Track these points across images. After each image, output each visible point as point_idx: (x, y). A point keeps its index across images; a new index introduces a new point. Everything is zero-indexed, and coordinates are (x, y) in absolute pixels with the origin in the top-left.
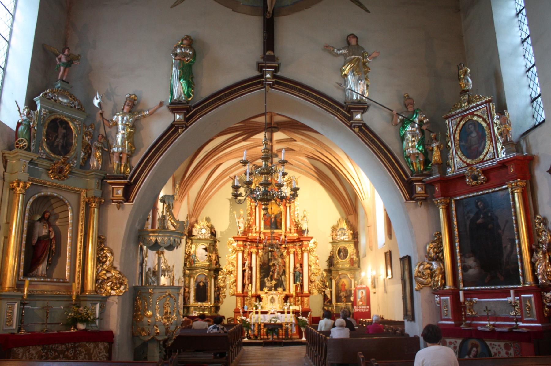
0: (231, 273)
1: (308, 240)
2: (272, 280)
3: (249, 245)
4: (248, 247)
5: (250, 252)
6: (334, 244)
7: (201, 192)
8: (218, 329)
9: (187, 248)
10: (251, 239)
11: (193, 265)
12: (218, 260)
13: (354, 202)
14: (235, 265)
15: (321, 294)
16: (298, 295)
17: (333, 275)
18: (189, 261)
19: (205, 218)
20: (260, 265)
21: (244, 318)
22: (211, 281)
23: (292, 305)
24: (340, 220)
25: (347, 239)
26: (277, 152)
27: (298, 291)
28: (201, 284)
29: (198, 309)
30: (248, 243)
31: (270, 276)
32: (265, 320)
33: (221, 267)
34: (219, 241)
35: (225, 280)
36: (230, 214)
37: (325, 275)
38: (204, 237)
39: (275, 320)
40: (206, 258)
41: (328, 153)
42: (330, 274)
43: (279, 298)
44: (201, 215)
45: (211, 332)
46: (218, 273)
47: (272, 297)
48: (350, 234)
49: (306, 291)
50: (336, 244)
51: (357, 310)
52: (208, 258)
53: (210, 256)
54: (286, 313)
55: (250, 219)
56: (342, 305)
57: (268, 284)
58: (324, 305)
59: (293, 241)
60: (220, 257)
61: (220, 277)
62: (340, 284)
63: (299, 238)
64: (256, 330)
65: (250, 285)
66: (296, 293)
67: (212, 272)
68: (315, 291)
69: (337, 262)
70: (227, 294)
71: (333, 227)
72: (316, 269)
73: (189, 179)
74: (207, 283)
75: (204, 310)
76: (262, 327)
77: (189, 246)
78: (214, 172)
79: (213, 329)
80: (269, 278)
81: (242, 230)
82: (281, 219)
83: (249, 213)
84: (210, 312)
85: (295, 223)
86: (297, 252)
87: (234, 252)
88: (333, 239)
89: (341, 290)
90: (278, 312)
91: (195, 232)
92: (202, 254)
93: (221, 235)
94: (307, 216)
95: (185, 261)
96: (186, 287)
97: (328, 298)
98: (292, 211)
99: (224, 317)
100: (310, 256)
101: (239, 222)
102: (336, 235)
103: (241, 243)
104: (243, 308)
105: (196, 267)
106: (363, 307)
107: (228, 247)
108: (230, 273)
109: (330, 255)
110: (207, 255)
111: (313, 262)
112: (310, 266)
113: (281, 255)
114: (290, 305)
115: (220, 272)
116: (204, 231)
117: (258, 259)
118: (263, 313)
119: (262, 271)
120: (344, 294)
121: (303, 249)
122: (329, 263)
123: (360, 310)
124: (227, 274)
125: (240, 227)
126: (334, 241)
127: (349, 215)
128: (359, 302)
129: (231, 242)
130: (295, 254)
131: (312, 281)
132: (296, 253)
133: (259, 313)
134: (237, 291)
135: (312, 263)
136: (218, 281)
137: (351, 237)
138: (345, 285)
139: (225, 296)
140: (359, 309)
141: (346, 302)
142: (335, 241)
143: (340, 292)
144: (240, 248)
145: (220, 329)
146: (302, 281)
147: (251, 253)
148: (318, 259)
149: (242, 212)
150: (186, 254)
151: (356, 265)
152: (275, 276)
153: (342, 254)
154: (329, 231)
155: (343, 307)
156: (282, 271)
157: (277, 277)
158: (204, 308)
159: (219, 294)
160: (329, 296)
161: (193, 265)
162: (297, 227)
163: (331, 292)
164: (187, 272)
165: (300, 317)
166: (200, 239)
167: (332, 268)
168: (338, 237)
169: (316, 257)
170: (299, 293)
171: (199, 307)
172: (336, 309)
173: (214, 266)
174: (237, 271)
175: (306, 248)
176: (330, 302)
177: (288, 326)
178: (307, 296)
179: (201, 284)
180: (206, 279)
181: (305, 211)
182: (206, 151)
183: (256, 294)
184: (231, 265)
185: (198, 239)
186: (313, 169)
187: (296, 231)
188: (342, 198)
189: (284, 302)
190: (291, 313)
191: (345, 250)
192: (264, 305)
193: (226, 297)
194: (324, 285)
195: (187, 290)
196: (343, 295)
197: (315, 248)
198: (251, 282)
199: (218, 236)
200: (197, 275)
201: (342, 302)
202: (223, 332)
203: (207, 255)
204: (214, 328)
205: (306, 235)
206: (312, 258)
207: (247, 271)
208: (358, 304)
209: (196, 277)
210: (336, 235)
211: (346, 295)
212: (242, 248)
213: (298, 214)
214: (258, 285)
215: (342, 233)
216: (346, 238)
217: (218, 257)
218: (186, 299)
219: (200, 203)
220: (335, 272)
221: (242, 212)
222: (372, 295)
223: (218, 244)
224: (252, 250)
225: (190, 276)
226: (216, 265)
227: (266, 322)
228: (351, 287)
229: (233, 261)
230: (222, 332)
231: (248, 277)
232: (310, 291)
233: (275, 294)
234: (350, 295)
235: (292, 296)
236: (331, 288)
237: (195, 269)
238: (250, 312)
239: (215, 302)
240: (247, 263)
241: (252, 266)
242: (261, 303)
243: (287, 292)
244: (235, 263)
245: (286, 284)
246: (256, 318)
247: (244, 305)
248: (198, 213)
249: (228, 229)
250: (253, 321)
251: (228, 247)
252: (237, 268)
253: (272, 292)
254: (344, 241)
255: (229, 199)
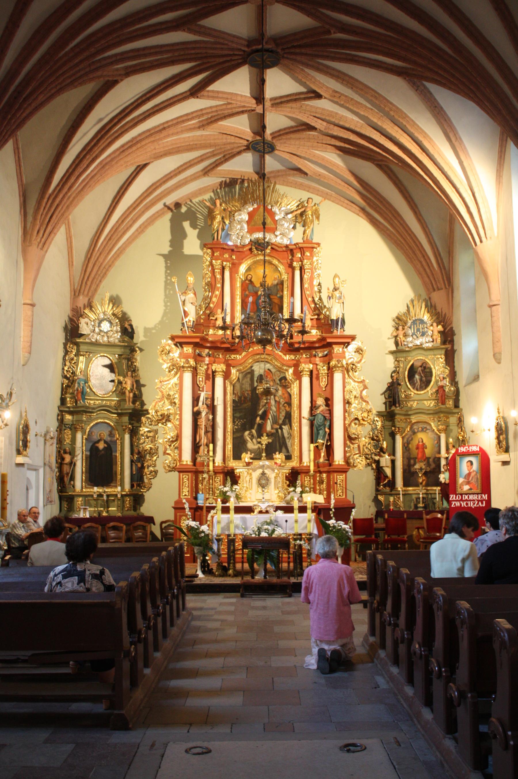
0: (168, 420)
1: (343, 343)
2: (260, 435)
3: (209, 355)
4: (207, 360)
5: (210, 372)
6: (399, 355)
7: (99, 238)
8: (82, 579)
9: (68, 363)
10: (212, 342)
11: (81, 403)
12: (140, 392)
13: (445, 261)
14: (177, 401)
15: (370, 468)
16: (322, 469)
17: (397, 424)
18: (72, 393)
19: (108, 295)
20: (234, 401)
21: (193, 524)
22: (122, 439)
23: (307, 492)
24: (412, 301)
25: (430, 345)
26: (273, 138)
27: (321, 460)
28: (101, 446)
29: (93, 502)
30: (207, 351)
31: (256, 427)
32: (246, 529)
33: (145, 407)
34: (141, 350)
35: (155, 437)
36: (166, 289)
37: (379, 424)
38: (105, 339)
39: (270, 528)
40: (111, 387)
41: (396, 128)
42: (390, 423)
43: (278, 474)
44: (99, 291)
45: (58, 589)
46: (139, 421)
47: (263, 474)
48: (436, 333)
49: (338, 458)
50: (404, 355)
51: (458, 504)
52: (117, 387)
53: (120, 383)
54: (296, 511)
55: (211, 299)
56: (420, 492)
57: (251, 445)
58: (378, 491)
59: (310, 347)
60: (144, 386)
61: (143, 430)
62: (413, 446)
63: (323, 339)
64: (224, 548)
65: (211, 446)
66: (317, 465)
67: (126, 419)
68: (360, 462)
69: (407, 397)
70: (159, 467)
71: (397, 318)
72: (361, 409)
73: (60, 190)
74: (115, 442)
75: (107, 505)
76: (239, 545)
77: (73, 359)
78: (126, 189)
79: (64, 577)
80: (254, 431)
81: (192, 318)
82: (282, 298)
83: (207, 284)
84: (122, 507)
85: (313, 306)
86: (318, 370)
87: (173, 372)
88: (397, 344)
89: (415, 459)
90: (277, 508)
91: (85, 328)
92: (102, 377)
93: (145, 336)
94: (341, 289)
95: (62, 394)
96: (65, 452)
97: (387, 477)
98: (305, 276)
99: (150, 520)
100: (348, 380)
101: (184, 302)
102: (405, 335)
103: (188, 350)
104: (196, 498)
105: (88, 407)
106: (471, 497)
107: (161, 361)
108: (165, 418)
109: (390, 380)
110: (113, 381)
111: (354, 393)
112: (349, 403)
113: (280, 380)
114: (302, 492)
115: (143, 419)
116: (105, 326)
117: (229, 389)
118: (239, 510)
119: (238, 415)
120: (424, 467)
121: (333, 363)
122: (389, 397)
123: (464, 504)
124: (158, 421)
125: (186, 314)
126: (400, 347)
127: (434, 290)
128: (462, 484)
129: (167, 348)
130: (314, 376)
131: (353, 436)
132: (315, 373)
133: (232, 512)
134: (180, 460)
135: (353, 397)
136: (139, 439)
137: (439, 340)
138: (424, 446)
139: (156, 472)
140: (462, 500)
141: (427, 485)
142: (404, 348)
143: (412, 462)
144: (188, 362)
145: (88, 578)
146: (331, 435)
147: (214, 372)
148: (365, 387)
149: (191, 279)
150: (65, 377)
151: (450, 403)
152: (269, 428)
153: (417, 377)
154: (389, 329)
155: (421, 496)
156: (283, 413)
157: (272, 428)
158: (107, 501)
159: (143, 467)
160: (388, 471)
161: (81, 403)
162: (318, 315)
163: (393, 462)
164: (68, 417)
165: (332, 522)
166: (97, 344)
167: (397, 410)
168: (410, 339)
169: (363, 382)
170: (324, 465)
171: (95, 496)
172: (404, 502)
173: (129, 405)
174: (181, 415)
175: (338, 361)
176: (392, 484)
177: (302, 542)
178: (343, 471)
179: (101, 446)
180: (111, 434)
181: (336, 276)
182: (101, 120)
183: (225, 467)
184: (167, 402)
185: (92, 344)
186: (355, 183)
187: (315, 322)
188: (418, 252)
189: (289, 486)
190: (309, 511)
191: (425, 368)
192: (243, 492)
193: (158, 474)
194: (376, 447)
195: (68, 458)
196: (421, 469)
197: (359, 362)
198: (213, 441)
199: (140, 337)
200: (92, 424)
201: (418, 486)
202: (102, 588)
203: (113, 381)
204: (67, 574)
205: (338, 332)
206: (353, 386)
207: (203, 414)
208: (459, 491)
209: (88, 430)
210: (405, 335)
211: (428, 469)
212: (192, 362)
213: (319, 284)
214: (230, 446)
215: (418, 330)
216: (425, 341)
217: (138, 385)
218: (66, 480)
219: (98, 264)
220: (403, 417)
221: (191, 279)
222: (495, 467)
223: (138, 356)
224: (214, 367)
225: (74, 428)
226: (134, 402)
227: (248, 532)
228: (439, 452)
229: (172, 393)
230: (96, 587)
231: (206, 428)
232: (347, 460)
233: (268, 467)
234: (437, 470)
235: (307, 472)
236: (393, 453)
237: (86, 412)
238: (210, 509)
239: (132, 486)
240: (203, 396)
241: (215, 403)
242: (235, 487)
243: (294, 463)
244: (177, 396)
245: (293, 445)
246: (223, 524)
247: (197, 492)
248: (94, 287)
249: (161, 322)
250: (217, 530)
251: (161, 361)
252: (181, 408)
253: (261, 463)
254: (423, 349)
255: (164, 256)
